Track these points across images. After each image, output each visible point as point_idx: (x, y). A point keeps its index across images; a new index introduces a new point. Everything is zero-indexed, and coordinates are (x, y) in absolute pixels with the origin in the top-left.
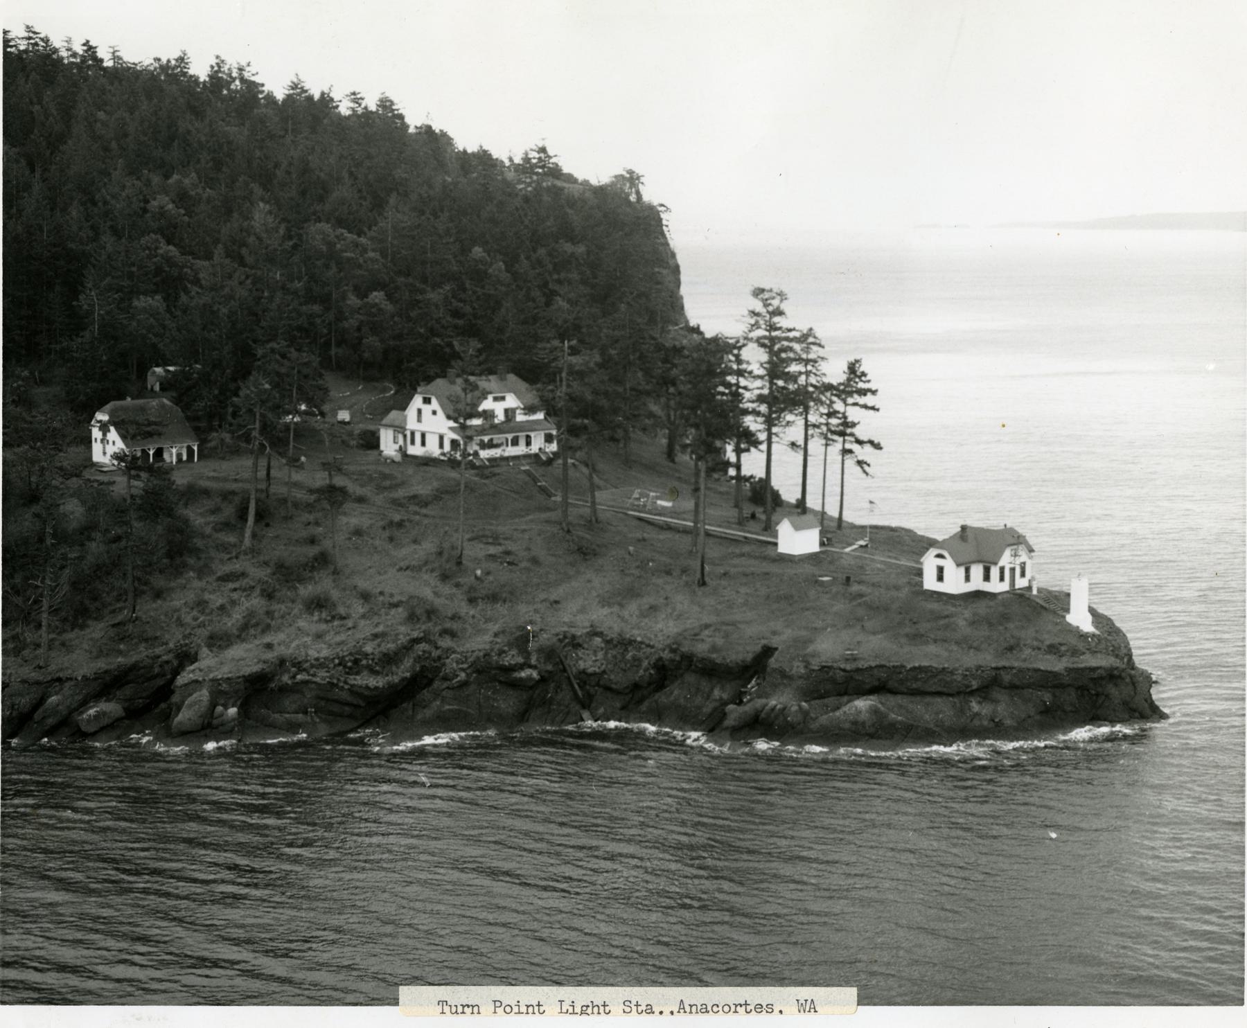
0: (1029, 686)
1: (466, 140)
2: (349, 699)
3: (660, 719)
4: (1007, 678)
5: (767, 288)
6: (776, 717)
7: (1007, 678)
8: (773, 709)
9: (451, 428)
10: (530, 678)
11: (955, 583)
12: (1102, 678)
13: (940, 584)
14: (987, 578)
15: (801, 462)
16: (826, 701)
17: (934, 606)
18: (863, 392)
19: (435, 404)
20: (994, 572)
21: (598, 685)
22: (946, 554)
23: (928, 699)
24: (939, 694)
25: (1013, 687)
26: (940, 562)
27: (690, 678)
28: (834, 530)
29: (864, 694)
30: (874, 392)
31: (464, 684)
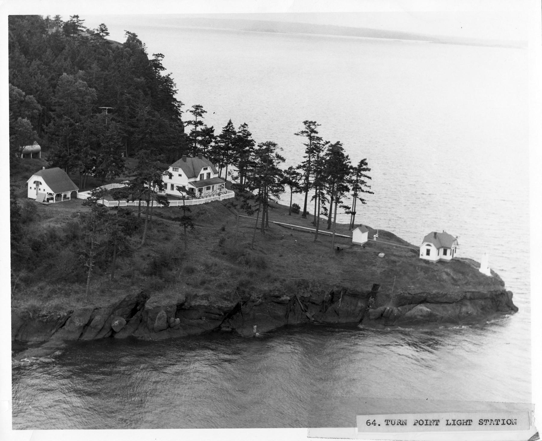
0: (477, 299)
1: (90, 24)
2: (218, 312)
3: (498, 310)
4: (468, 295)
5: (178, 100)
6: (390, 314)
7: (468, 295)
8: (389, 310)
9: (190, 183)
10: (286, 300)
11: (434, 257)
12: (499, 295)
13: (428, 256)
14: (445, 253)
15: (304, 199)
16: (405, 306)
17: (424, 264)
18: (365, 170)
19: (180, 171)
20: (448, 252)
21: (309, 301)
22: (432, 244)
23: (443, 305)
24: (446, 303)
25: (471, 299)
26: (429, 247)
27: (347, 298)
28: (371, 232)
29: (418, 304)
30: (369, 170)
31: (261, 304)
